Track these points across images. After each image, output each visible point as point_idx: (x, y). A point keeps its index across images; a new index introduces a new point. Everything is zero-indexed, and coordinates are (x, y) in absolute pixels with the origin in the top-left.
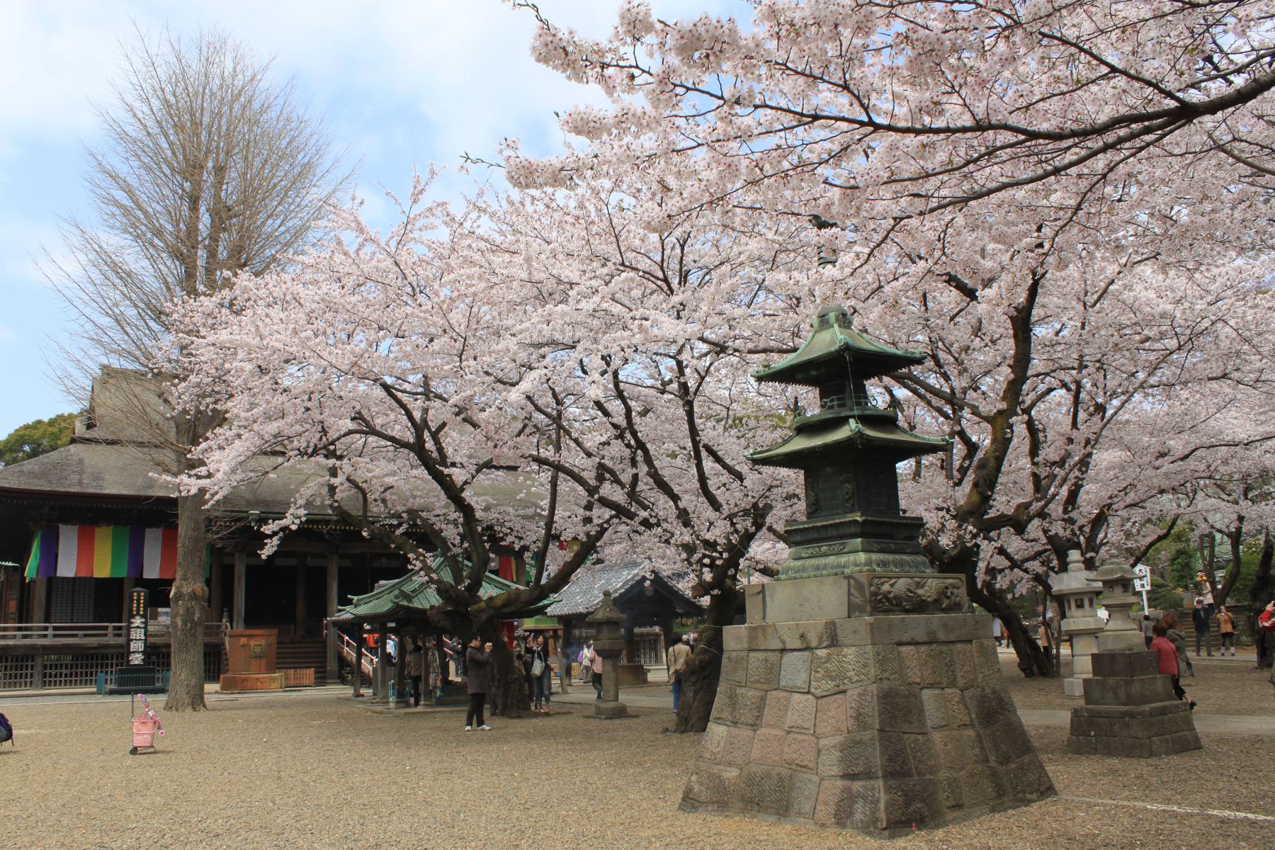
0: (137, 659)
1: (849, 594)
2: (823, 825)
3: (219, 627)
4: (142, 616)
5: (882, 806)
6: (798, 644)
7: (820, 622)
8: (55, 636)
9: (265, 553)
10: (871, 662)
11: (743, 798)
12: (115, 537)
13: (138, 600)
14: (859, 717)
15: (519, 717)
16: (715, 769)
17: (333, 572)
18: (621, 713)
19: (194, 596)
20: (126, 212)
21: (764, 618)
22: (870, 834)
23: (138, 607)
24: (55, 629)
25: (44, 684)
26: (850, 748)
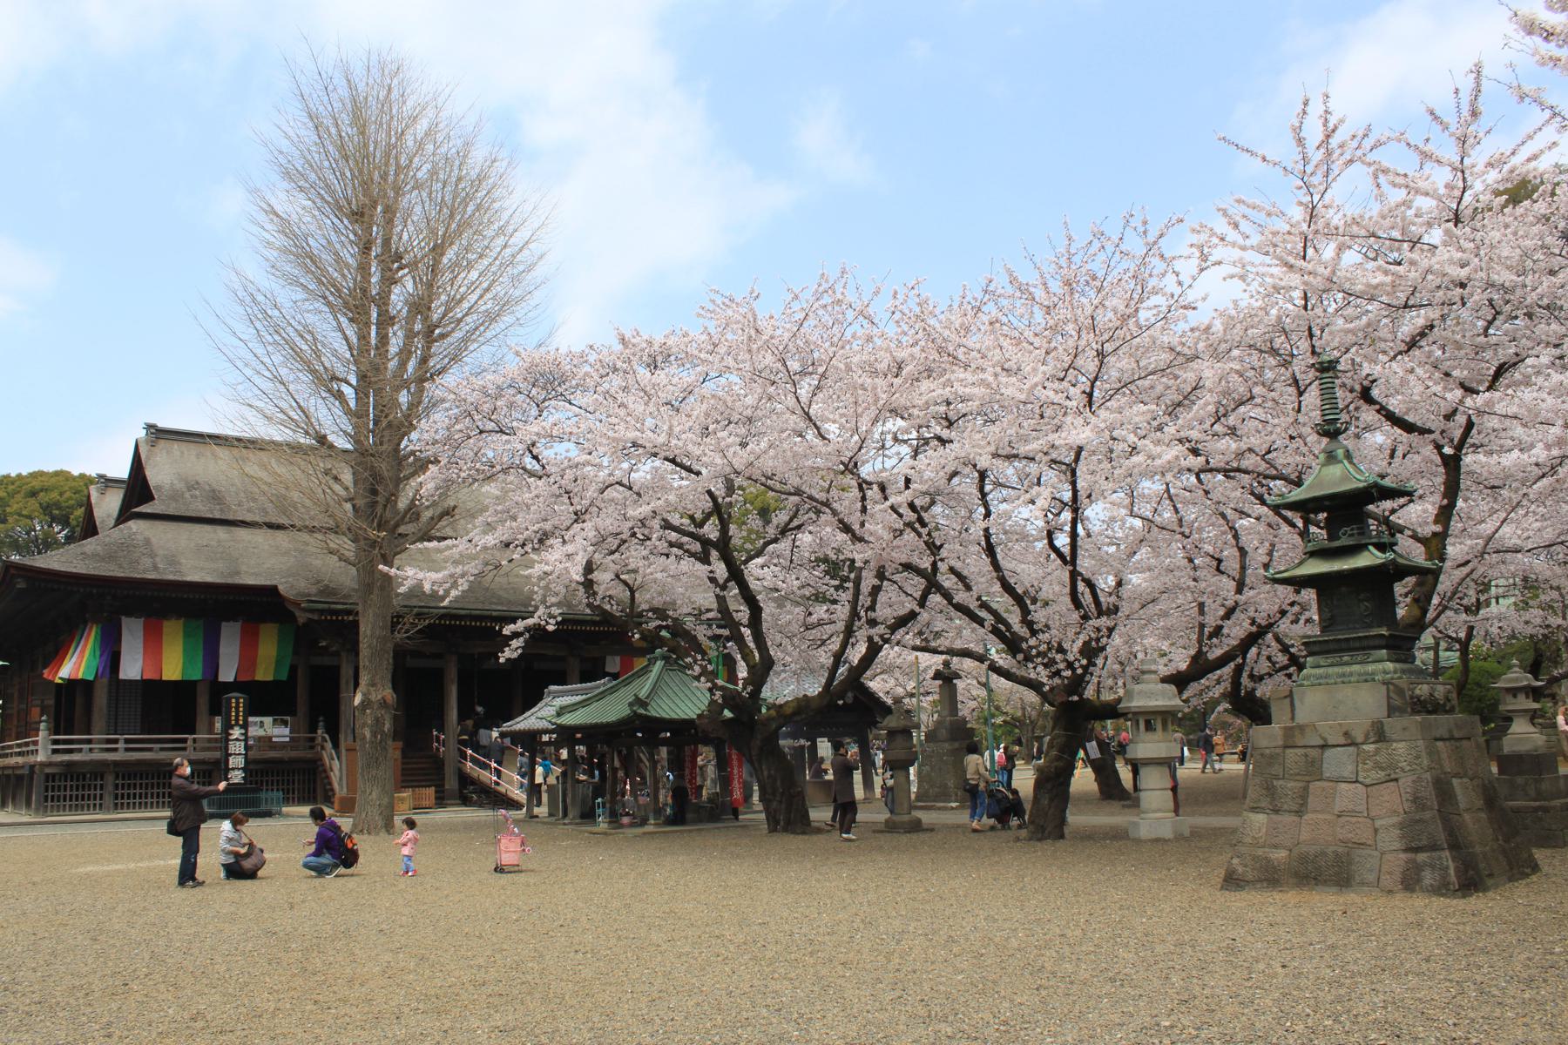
1: (1389, 698)
2: (1390, 891)
3: (313, 739)
4: (242, 727)
5: (1452, 871)
6: (1342, 741)
7: (1366, 723)
8: (127, 750)
9: (509, 653)
10: (1424, 754)
11: (1296, 874)
12: (187, 635)
13: (237, 708)
14: (1415, 800)
15: (804, 833)
16: (1260, 852)
17: (452, 673)
18: (916, 827)
19: (383, 704)
20: (297, 256)
21: (1293, 719)
22: (1443, 895)
23: (237, 716)
24: (127, 741)
26: (1409, 827)
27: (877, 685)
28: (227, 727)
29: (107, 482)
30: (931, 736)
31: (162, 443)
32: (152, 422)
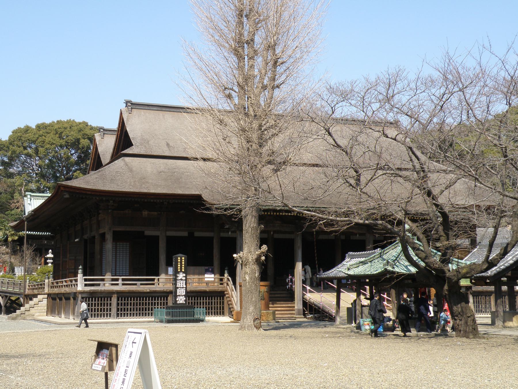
0: (181, 300)
4: (184, 273)
8: (123, 284)
23: (181, 267)
24: (123, 280)
25: (118, 315)
27: (478, 229)
28: (176, 272)
29: (105, 131)
30: (103, 236)
32: (128, 99)
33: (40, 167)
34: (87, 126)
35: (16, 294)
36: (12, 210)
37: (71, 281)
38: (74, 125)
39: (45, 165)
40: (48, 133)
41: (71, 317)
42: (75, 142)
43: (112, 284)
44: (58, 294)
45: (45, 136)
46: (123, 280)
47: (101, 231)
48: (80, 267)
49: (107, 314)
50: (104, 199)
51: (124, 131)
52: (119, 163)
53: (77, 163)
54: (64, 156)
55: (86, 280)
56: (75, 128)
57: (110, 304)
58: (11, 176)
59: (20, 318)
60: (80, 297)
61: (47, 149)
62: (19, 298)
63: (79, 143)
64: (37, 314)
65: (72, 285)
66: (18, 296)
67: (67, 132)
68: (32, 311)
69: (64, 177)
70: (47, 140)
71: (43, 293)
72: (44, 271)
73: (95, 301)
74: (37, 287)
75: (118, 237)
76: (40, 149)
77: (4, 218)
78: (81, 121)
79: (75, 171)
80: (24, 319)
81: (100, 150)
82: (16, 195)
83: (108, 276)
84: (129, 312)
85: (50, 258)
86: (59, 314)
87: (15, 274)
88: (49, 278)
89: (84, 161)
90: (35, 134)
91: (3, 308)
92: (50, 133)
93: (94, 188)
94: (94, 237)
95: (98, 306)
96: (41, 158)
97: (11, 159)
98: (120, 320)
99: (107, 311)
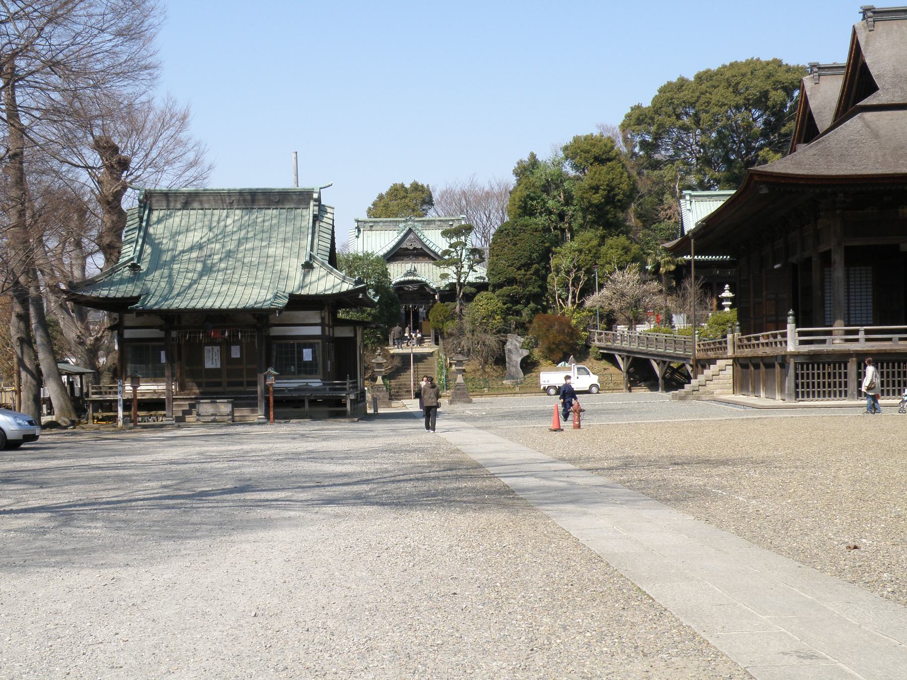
8: (867, 340)
24: (867, 332)
29: (820, 70)
30: (826, 260)
31: (880, 26)
33: (702, 146)
34: (780, 66)
35: (678, 358)
36: (660, 222)
37: (775, 336)
38: (759, 66)
39: (710, 143)
40: (715, 87)
41: (778, 397)
42: (760, 98)
43: (847, 340)
44: (751, 358)
45: (710, 93)
46: (867, 332)
47: (823, 248)
48: (791, 312)
49: (840, 392)
50: (830, 190)
51: (859, 65)
52: (854, 124)
53: (764, 134)
54: (743, 124)
55: (801, 334)
56: (760, 73)
57: (846, 374)
58: (656, 165)
59: (691, 397)
60: (792, 362)
61: (714, 115)
62: (683, 365)
63: (767, 99)
64: (718, 391)
65: (776, 343)
66: (681, 362)
67: (746, 82)
68: (710, 386)
69: (743, 160)
70: (714, 99)
71: (725, 356)
72: (720, 321)
73: (818, 369)
74: (712, 346)
75: (853, 258)
76: (703, 116)
77: (649, 235)
78: (771, 59)
79: (761, 148)
80: (698, 399)
81: (813, 104)
82: (667, 196)
83: (839, 327)
84: (816, 389)
85: (727, 299)
86: (756, 391)
87: (674, 327)
88: (733, 332)
89: (776, 128)
90: (693, 92)
91: (660, 381)
92: (718, 86)
93: (811, 172)
94: (809, 260)
95: (824, 378)
96: (703, 132)
97: (657, 137)
98: (801, 403)
99: (840, 387)
